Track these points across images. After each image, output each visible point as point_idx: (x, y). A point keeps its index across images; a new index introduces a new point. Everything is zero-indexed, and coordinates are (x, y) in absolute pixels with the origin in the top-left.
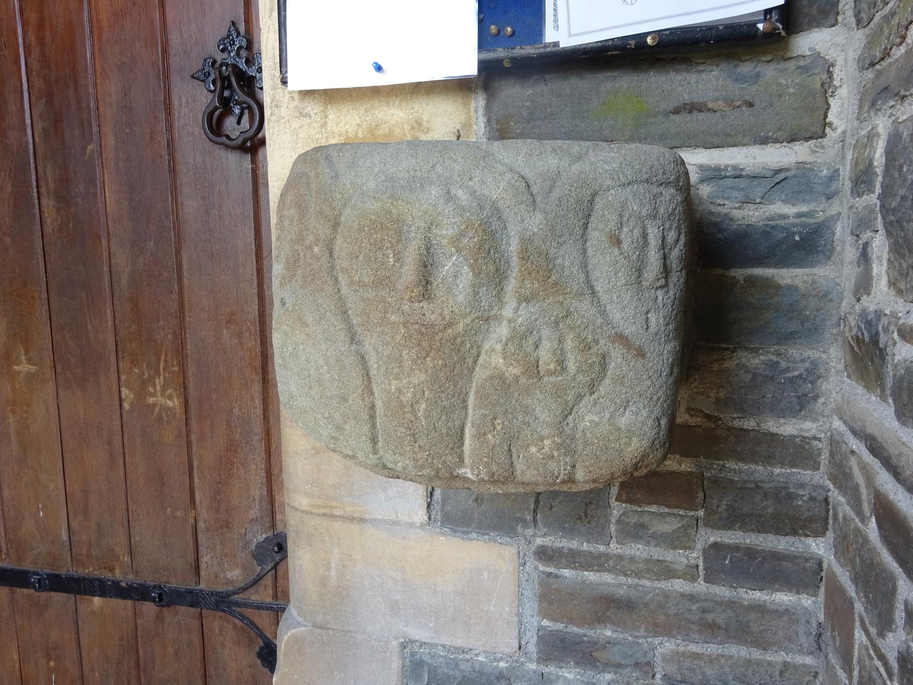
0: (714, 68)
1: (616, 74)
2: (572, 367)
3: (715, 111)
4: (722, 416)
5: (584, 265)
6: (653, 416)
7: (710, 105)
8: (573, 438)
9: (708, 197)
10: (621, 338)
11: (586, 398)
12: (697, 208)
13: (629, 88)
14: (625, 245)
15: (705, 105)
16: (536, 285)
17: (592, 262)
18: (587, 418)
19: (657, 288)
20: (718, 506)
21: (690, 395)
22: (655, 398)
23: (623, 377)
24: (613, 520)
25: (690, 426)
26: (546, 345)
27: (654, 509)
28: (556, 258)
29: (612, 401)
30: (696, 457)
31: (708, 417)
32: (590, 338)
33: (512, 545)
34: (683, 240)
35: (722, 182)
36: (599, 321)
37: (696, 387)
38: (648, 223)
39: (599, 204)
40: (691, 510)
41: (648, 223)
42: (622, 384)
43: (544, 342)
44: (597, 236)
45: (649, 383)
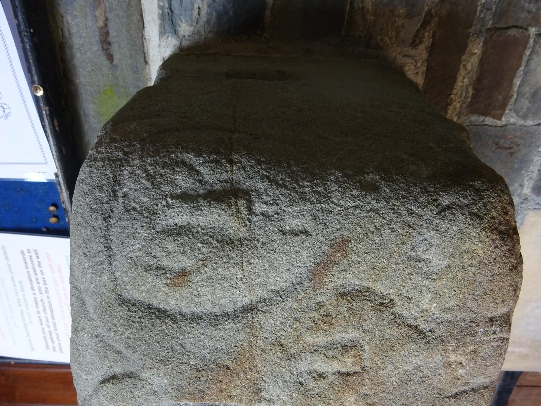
0: (65, 20)
1: (82, 114)
2: (352, 335)
3: (107, 19)
4: (426, 9)
5: (214, 319)
6: (436, 221)
7: (101, 24)
8: (452, 324)
9: (192, 25)
10: (318, 271)
11: (397, 309)
12: (203, 37)
13: (93, 103)
14: (188, 263)
15: (101, 29)
16: (238, 383)
17: (209, 308)
18: (426, 306)
19: (250, 209)
20: (529, 12)
21: (398, 46)
22: (409, 219)
23: (374, 268)
24: (521, 122)
25: (433, 44)
26: (321, 364)
27: (517, 82)
28: (203, 357)
29: (406, 279)
30: (468, 37)
31: (425, 24)
32: (314, 315)
33: (525, 215)
34: (191, 158)
35: (176, 11)
36: (290, 304)
37: (390, 38)
38: (161, 224)
39: (133, 294)
40: (527, 42)
41: (161, 224)
42: (384, 269)
43: (315, 367)
44: (174, 301)
45: (386, 232)
